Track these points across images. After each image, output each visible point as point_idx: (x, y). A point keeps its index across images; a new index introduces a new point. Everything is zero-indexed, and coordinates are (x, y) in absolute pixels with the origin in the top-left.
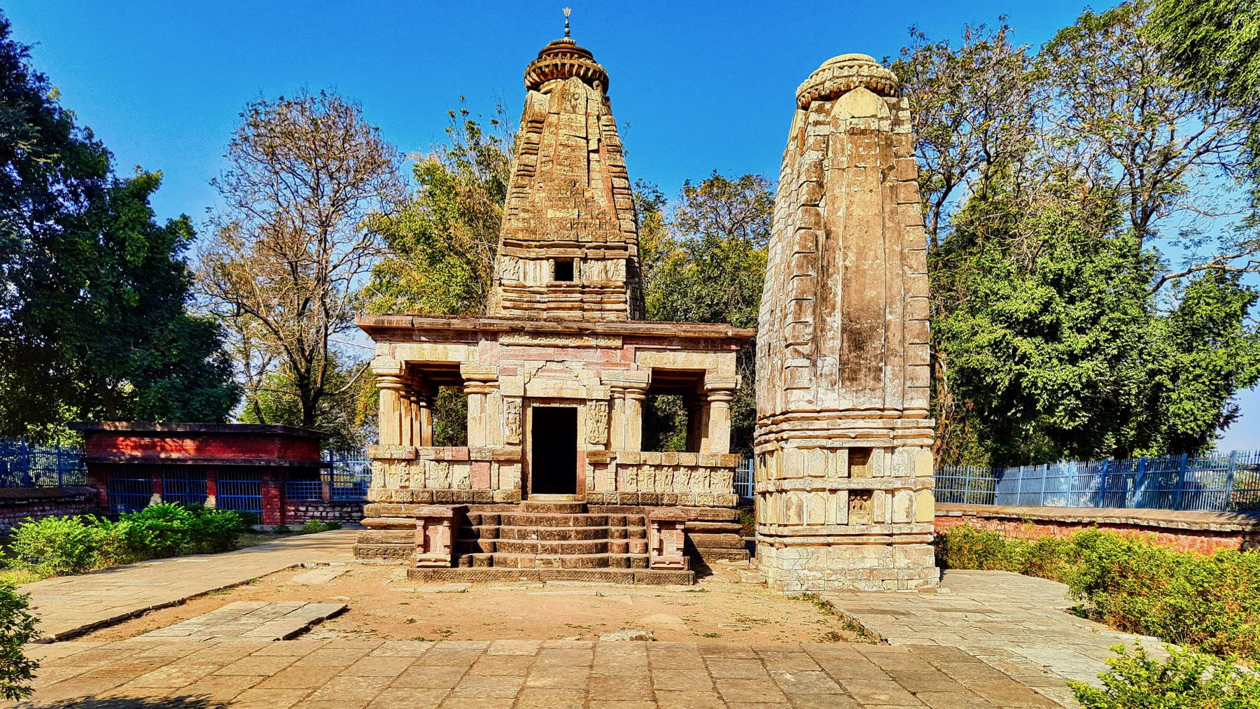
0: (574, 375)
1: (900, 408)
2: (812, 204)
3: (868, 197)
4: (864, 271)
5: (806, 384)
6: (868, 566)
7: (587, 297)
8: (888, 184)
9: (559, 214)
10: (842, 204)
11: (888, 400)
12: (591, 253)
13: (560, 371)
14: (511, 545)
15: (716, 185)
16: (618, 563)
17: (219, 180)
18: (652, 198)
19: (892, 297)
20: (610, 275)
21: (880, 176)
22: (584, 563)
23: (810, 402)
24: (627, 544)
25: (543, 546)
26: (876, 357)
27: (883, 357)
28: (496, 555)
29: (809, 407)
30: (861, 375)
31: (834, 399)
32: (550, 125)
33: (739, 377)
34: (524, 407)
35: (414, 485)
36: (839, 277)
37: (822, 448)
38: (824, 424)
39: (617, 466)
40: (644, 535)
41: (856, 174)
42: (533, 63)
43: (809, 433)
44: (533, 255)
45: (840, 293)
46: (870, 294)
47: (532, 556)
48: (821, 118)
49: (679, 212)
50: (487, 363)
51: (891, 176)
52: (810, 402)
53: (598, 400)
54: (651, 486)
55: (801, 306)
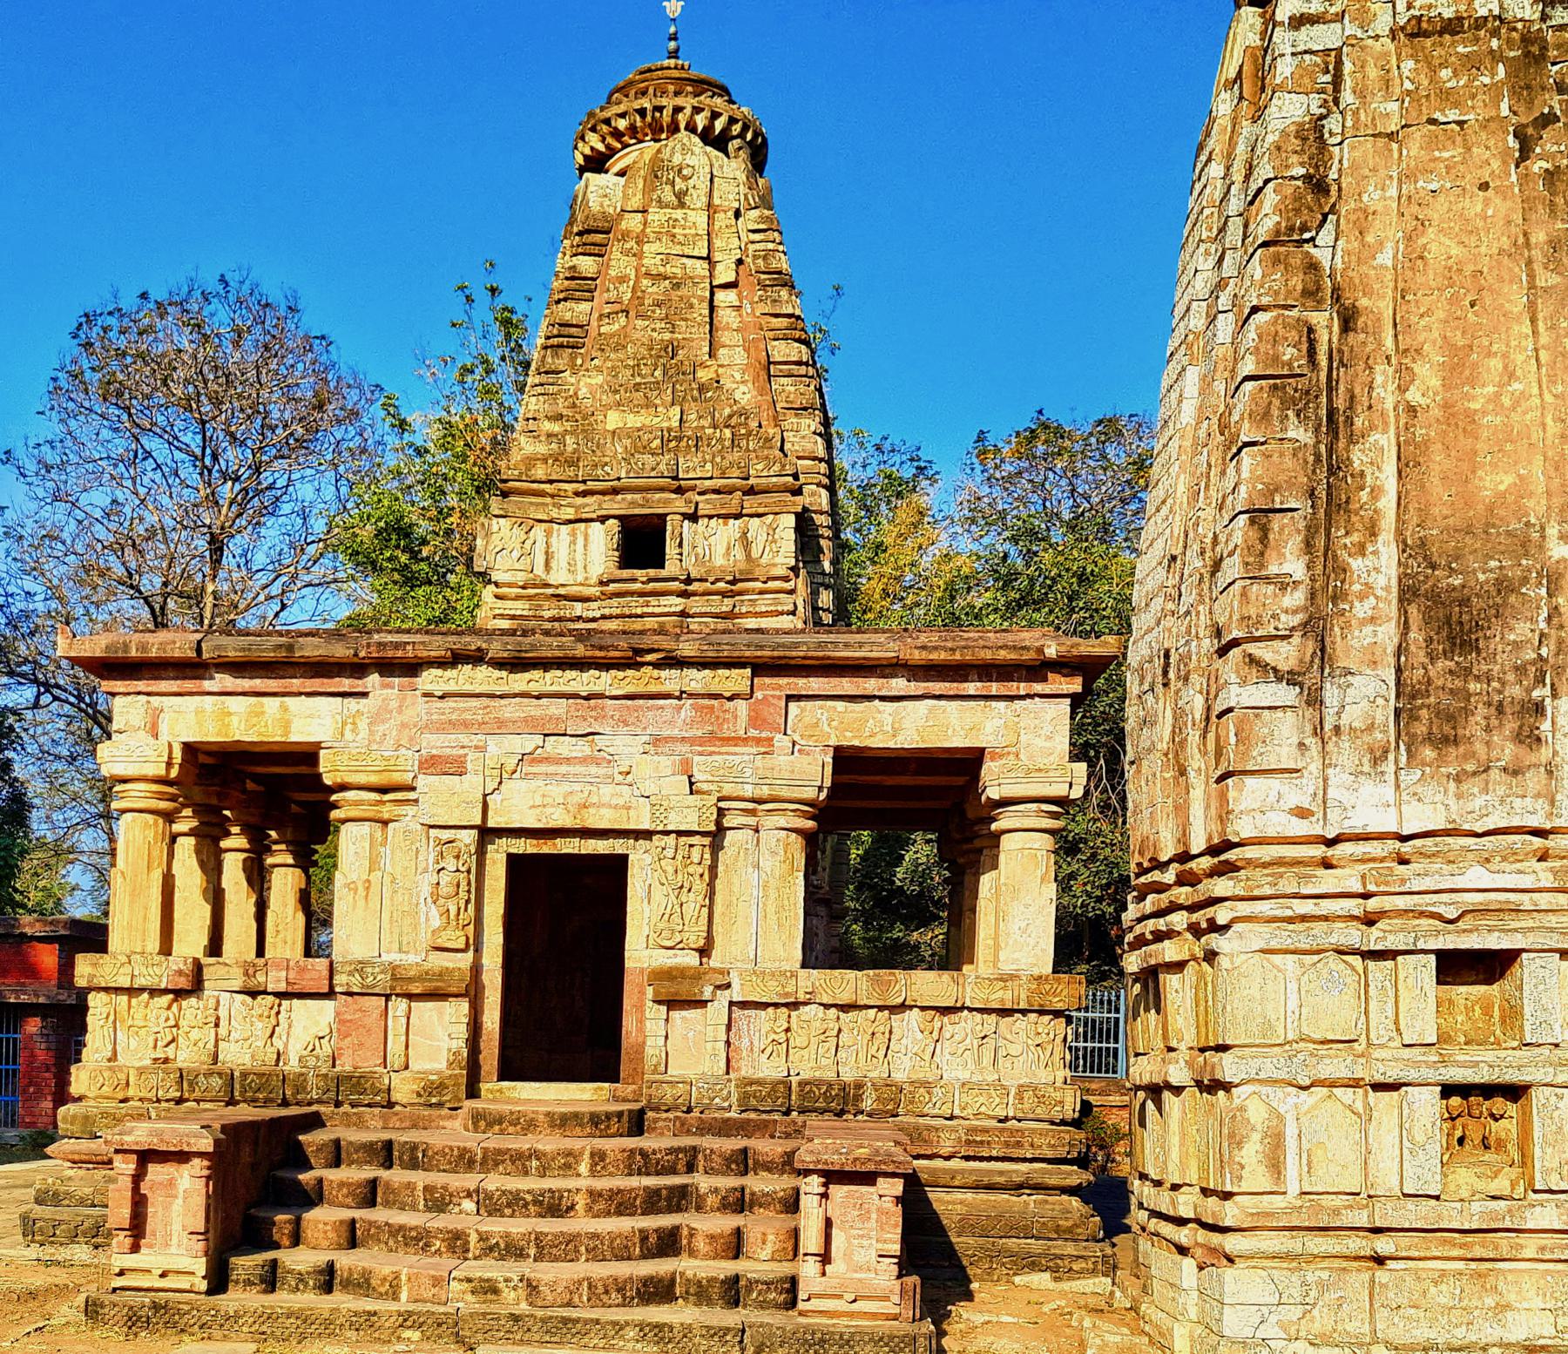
0: (608, 771)
2: (1289, 239)
3: (1475, 205)
4: (1470, 416)
5: (1285, 756)
7: (696, 604)
8: (1538, 166)
9: (634, 421)
12: (706, 505)
13: (584, 761)
14: (397, 1231)
15: (1043, 435)
16: (701, 1293)
17: (20, 453)
18: (908, 472)
21: (1512, 142)
22: (598, 1292)
23: (1302, 813)
24: (738, 1233)
25: (483, 1238)
26: (1520, 670)
28: (346, 1261)
29: (1300, 828)
30: (1475, 725)
32: (625, 236)
33: (1082, 768)
34: (481, 852)
35: (187, 1056)
36: (1386, 441)
40: (792, 1204)
41: (1431, 143)
42: (591, 115)
43: (1306, 907)
44: (569, 513)
45: (1391, 485)
46: (1494, 482)
47: (448, 1262)
49: (964, 496)
50: (390, 742)
52: (1302, 813)
53: (680, 833)
55: (1265, 532)
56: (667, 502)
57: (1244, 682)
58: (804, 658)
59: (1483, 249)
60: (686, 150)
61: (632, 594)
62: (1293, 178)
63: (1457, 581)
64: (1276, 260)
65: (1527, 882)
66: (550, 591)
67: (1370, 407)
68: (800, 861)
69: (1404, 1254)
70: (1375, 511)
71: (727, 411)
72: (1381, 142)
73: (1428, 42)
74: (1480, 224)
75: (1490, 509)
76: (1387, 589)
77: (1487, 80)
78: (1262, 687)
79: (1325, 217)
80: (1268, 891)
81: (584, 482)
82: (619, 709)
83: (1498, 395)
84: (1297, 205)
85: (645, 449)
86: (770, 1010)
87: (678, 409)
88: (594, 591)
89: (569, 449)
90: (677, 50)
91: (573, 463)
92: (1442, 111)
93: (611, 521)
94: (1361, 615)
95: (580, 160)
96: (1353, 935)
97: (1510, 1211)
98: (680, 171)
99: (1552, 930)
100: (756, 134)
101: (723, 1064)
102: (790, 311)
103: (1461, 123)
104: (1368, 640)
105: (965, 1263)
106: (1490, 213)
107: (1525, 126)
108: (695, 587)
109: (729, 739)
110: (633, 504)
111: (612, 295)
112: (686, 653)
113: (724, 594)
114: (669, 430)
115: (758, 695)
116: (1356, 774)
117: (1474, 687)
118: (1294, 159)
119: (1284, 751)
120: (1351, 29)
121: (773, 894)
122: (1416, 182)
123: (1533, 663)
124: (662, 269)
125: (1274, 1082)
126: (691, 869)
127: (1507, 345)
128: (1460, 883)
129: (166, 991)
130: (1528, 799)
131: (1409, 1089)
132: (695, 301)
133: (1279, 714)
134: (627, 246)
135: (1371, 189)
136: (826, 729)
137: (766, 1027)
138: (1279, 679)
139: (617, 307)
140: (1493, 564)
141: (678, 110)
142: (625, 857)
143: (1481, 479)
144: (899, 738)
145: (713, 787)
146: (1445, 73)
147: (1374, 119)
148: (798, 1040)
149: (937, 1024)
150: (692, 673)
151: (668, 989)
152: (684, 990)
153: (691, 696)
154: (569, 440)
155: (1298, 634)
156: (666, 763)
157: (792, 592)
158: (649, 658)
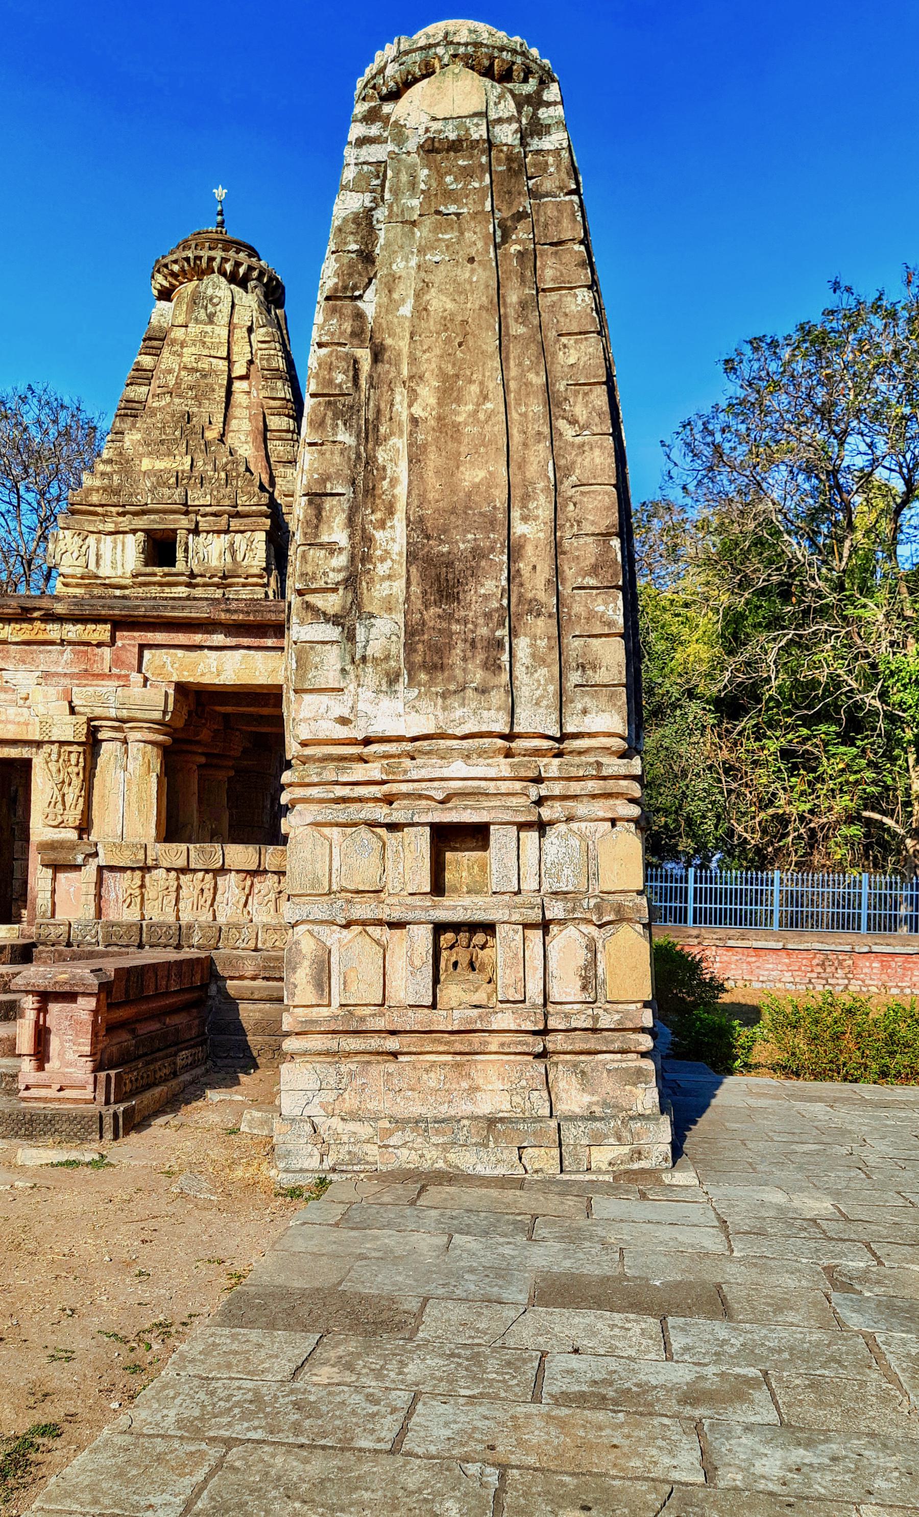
1: (554, 731)
3: (464, 273)
4: (456, 426)
6: (484, 1109)
7: (199, 592)
9: (160, 465)
10: (406, 290)
11: (522, 713)
19: (527, 483)
20: (239, 558)
23: (344, 721)
26: (488, 616)
27: (510, 619)
29: (343, 732)
31: (395, 713)
32: (173, 342)
36: (400, 443)
37: (372, 825)
38: (374, 771)
39: (100, 869)
42: (157, 261)
43: (345, 791)
44: (110, 527)
45: (402, 470)
48: (374, 130)
51: (522, 233)
52: (344, 721)
53: (62, 743)
54: (170, 910)
55: (319, 510)
56: (176, 521)
57: (302, 623)
58: (144, 616)
59: (469, 305)
60: (216, 286)
61: (154, 584)
62: (349, 252)
63: (445, 549)
64: (334, 310)
65: (492, 773)
66: (99, 582)
67: (391, 419)
68: (157, 766)
69: (405, 1050)
70: (393, 496)
71: (225, 460)
72: (407, 228)
73: (439, 157)
74: (468, 287)
75: (469, 495)
76: (400, 554)
77: (477, 185)
78: (315, 626)
79: (370, 280)
80: (315, 779)
81: (124, 506)
82: (20, 651)
83: (476, 412)
84: (350, 271)
85: (165, 484)
86: (129, 872)
87: (189, 458)
88: (128, 582)
89: (115, 484)
90: (223, 222)
91: (117, 492)
92: (446, 206)
93: (140, 533)
94: (381, 573)
95: (156, 293)
96: (381, 813)
97: (480, 1016)
98: (211, 300)
99: (508, 808)
100: (271, 279)
101: (92, 911)
102: (283, 395)
103: (458, 215)
104: (386, 592)
105: (255, 1054)
106: (475, 279)
107: (506, 220)
108: (199, 580)
109: (98, 675)
110: (153, 521)
111: (162, 382)
112: (59, 611)
113: (218, 586)
114: (183, 471)
115: (119, 643)
116: (378, 692)
117: (455, 627)
118: (351, 238)
119: (331, 674)
120: (390, 147)
121: (135, 789)
122: (425, 255)
123: (497, 610)
124: (195, 365)
125: (322, 922)
126: (70, 770)
127: (484, 376)
128: (446, 773)
129: (201, 870)
130: (493, 712)
131: (411, 926)
132: (216, 387)
133: (328, 647)
134: (174, 349)
135: (399, 260)
136: (170, 668)
137: (126, 885)
138: (327, 621)
139: (165, 390)
140: (470, 536)
141: (211, 259)
142: (29, 761)
143: (462, 473)
144: (222, 677)
145: (87, 710)
146: (449, 179)
147: (403, 211)
148: (150, 893)
149: (248, 883)
150: (69, 627)
151: (52, 856)
152: (62, 857)
153: (71, 643)
154: (115, 477)
155: (341, 587)
156: (53, 692)
157: (264, 585)
158: (36, 614)
